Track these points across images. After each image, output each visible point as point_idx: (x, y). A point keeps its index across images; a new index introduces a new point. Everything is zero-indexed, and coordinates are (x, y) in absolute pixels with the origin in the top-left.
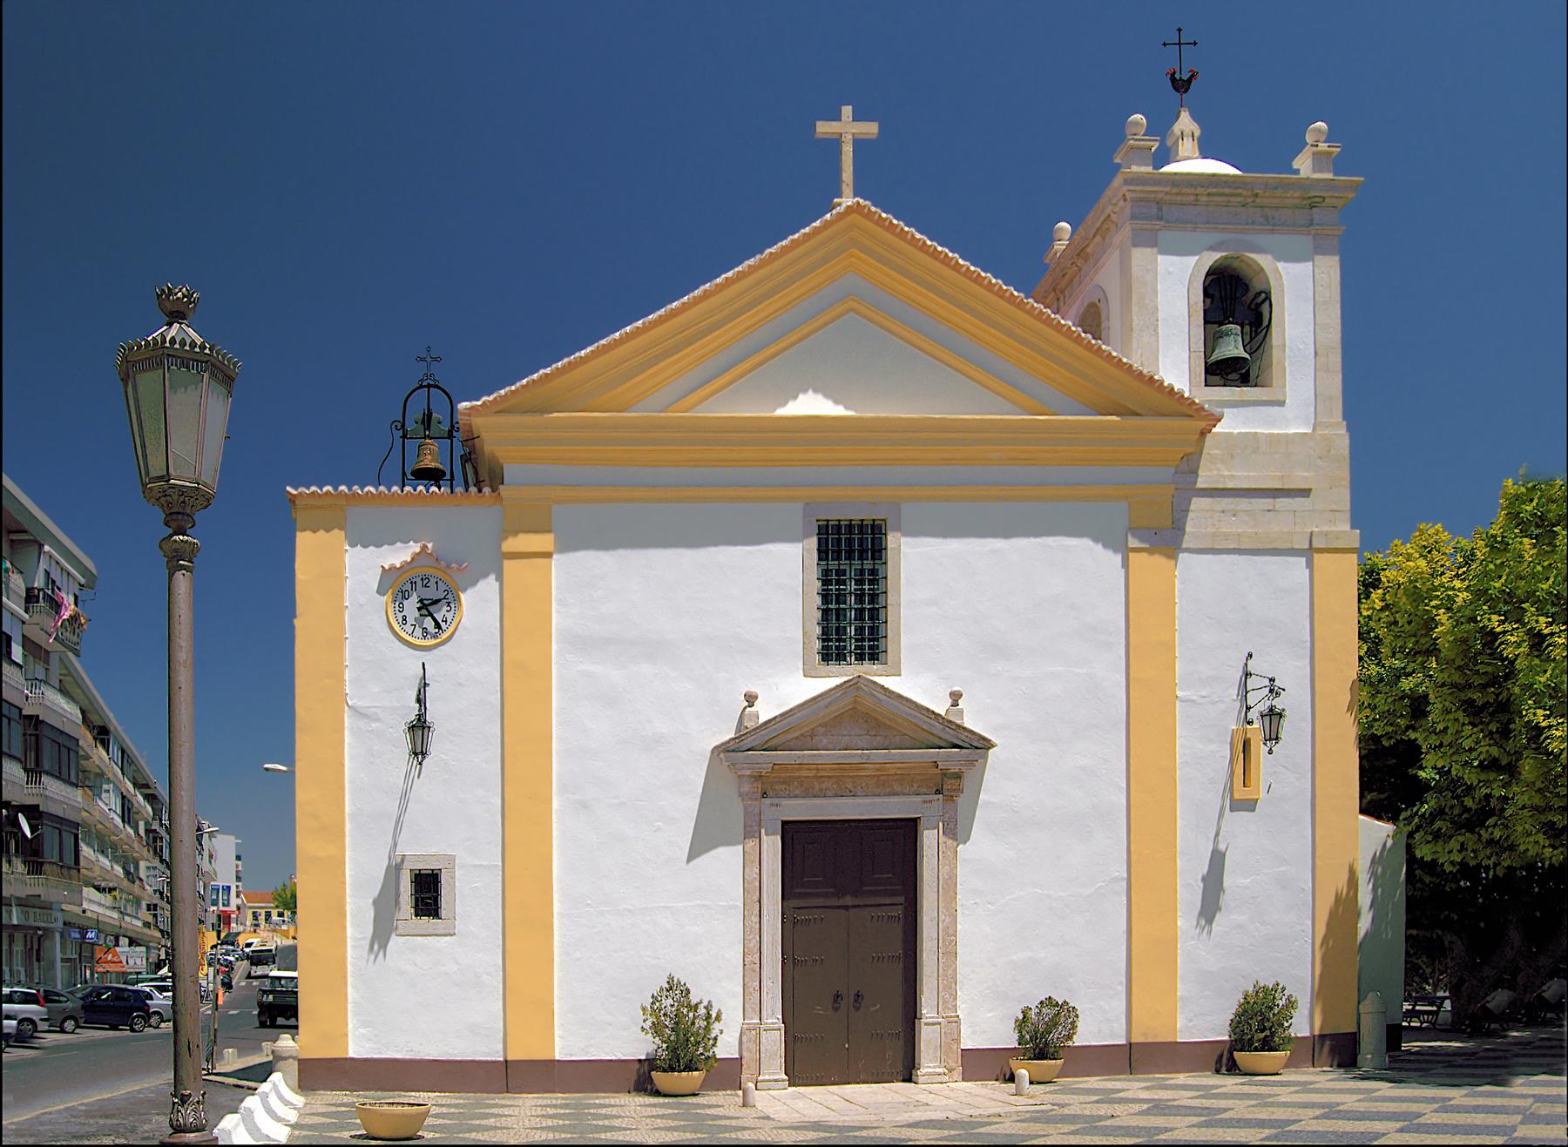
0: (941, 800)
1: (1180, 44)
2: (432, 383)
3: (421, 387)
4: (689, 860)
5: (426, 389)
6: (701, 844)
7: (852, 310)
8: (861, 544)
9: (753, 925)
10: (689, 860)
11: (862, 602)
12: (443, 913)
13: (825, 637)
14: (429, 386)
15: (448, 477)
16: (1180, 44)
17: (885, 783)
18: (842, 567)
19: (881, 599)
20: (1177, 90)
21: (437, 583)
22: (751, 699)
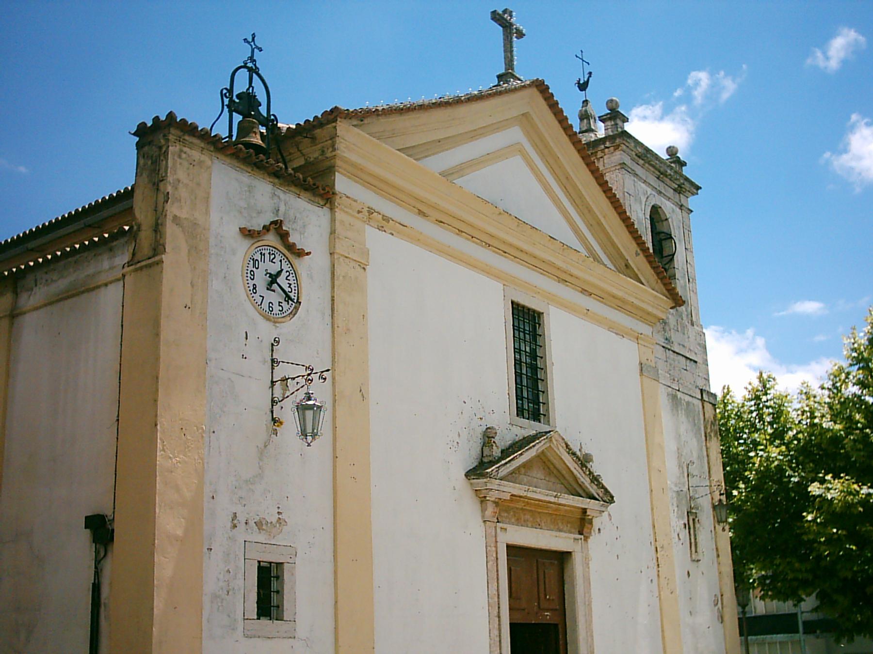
21: (281, 261)
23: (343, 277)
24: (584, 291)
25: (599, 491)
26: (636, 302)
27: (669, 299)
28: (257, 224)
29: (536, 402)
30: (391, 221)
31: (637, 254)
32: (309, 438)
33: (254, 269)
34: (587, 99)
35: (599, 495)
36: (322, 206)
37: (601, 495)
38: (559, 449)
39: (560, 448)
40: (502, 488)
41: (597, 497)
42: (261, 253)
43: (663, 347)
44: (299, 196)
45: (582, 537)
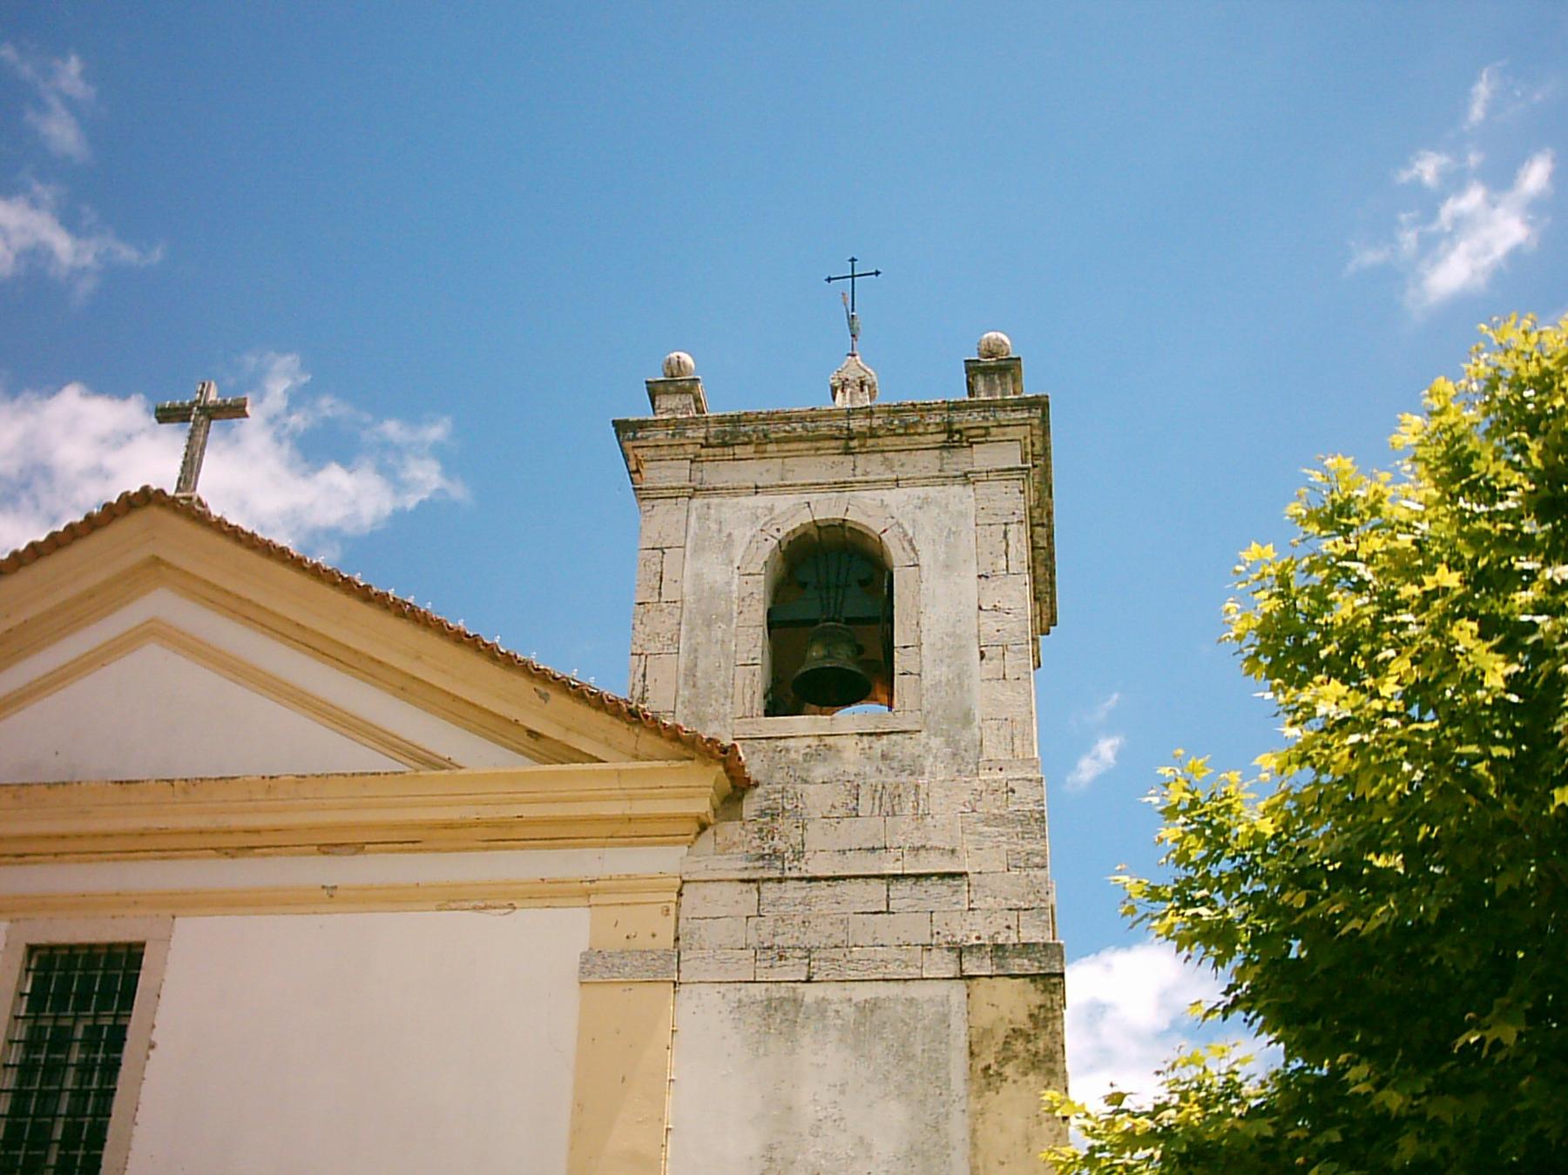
7: (153, 631)
16: (853, 276)
27: (692, 759)
31: (544, 697)
43: (743, 881)
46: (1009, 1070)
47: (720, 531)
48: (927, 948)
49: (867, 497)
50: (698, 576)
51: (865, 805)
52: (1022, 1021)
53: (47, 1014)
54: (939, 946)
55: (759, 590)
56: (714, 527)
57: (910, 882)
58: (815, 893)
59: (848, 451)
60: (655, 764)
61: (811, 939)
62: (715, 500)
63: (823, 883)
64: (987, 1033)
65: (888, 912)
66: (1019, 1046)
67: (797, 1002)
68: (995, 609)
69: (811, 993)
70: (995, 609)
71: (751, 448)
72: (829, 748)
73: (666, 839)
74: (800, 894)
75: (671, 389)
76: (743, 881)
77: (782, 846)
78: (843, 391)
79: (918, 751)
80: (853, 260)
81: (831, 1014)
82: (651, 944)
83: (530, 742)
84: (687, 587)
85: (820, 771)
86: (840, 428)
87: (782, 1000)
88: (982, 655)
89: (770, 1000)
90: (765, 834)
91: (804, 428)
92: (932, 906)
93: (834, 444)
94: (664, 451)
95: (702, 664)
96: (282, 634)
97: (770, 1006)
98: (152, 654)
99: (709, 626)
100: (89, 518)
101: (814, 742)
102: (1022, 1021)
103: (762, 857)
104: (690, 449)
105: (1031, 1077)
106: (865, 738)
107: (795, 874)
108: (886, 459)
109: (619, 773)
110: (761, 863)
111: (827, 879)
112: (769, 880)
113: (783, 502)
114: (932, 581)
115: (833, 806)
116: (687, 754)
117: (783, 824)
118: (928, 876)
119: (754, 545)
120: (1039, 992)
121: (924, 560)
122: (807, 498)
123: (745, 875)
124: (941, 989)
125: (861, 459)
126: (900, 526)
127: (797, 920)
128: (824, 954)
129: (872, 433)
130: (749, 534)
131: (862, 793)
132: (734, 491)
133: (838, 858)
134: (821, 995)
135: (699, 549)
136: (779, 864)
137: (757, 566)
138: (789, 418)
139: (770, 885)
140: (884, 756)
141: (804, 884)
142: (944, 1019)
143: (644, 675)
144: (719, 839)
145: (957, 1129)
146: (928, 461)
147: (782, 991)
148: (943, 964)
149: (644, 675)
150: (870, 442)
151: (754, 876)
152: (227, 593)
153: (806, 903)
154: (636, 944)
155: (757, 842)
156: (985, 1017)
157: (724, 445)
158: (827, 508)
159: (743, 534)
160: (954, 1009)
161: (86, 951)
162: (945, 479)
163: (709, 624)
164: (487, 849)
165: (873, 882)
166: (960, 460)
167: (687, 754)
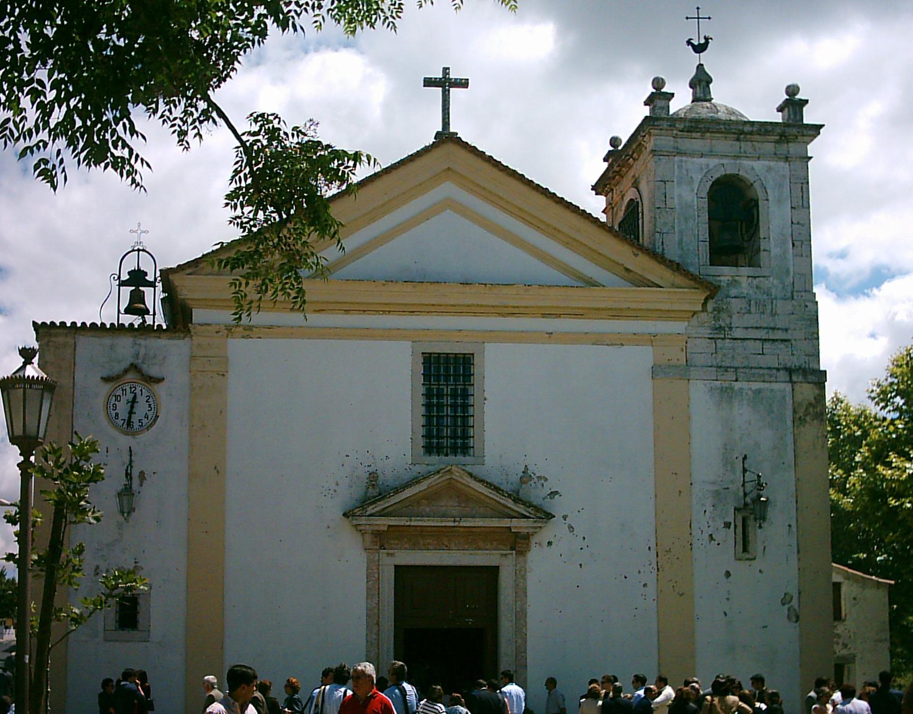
0: (514, 555)
1: (698, 18)
2: (141, 248)
3: (133, 250)
4: (823, 125)
5: (137, 252)
6: (817, 129)
7: (449, 204)
8: (455, 371)
9: (373, 641)
10: (823, 125)
11: (456, 412)
12: (140, 627)
13: (428, 436)
14: (139, 250)
15: (152, 313)
16: (698, 18)
17: (473, 538)
18: (441, 387)
19: (471, 410)
20: (696, 52)
21: (141, 390)
22: (711, 39)
23: (200, 388)
24: (544, 316)
25: (530, 510)
26: (632, 306)
27: (698, 288)
28: (118, 368)
29: (465, 436)
30: (254, 329)
31: (636, 255)
32: (126, 515)
33: (117, 403)
34: (702, 63)
35: (530, 513)
36: (184, 338)
37: (532, 512)
38: (463, 478)
39: (465, 477)
40: (372, 522)
41: (528, 514)
42: (123, 390)
43: (709, 338)
44: (159, 338)
45: (514, 552)
46: (808, 418)
47: (687, 175)
48: (778, 369)
49: (746, 163)
50: (680, 196)
51: (753, 309)
52: (812, 400)
53: (452, 383)
54: (782, 369)
55: (704, 204)
56: (685, 172)
57: (771, 342)
58: (736, 345)
59: (738, 140)
60: (685, 290)
61: (736, 364)
62: (684, 158)
63: (739, 341)
64: (800, 404)
65: (763, 354)
66: (811, 410)
67: (732, 389)
68: (798, 223)
69: (737, 385)
70: (798, 223)
71: (699, 134)
72: (736, 281)
73: (680, 319)
74: (730, 345)
75: (662, 97)
76: (709, 338)
77: (723, 325)
78: (700, 86)
79: (770, 285)
80: (698, 8)
81: (744, 394)
82: (679, 363)
83: (623, 272)
84: (676, 201)
85: (733, 292)
86: (739, 130)
87: (727, 388)
88: (793, 245)
89: (722, 387)
90: (716, 318)
91: (725, 128)
92: (778, 351)
93: (733, 136)
94: (663, 132)
95: (684, 239)
96: (511, 212)
97: (723, 390)
98: (448, 215)
99: (686, 222)
100: (584, 211)
101: (730, 279)
102: (812, 400)
103: (716, 329)
104: (675, 132)
105: (815, 422)
106: (750, 279)
107: (730, 337)
108: (753, 145)
109: (670, 292)
110: (716, 332)
111: (740, 339)
112: (719, 338)
113: (713, 162)
114: (773, 208)
115: (741, 309)
116: (697, 286)
117: (724, 315)
118: (777, 340)
119: (702, 184)
120: (83, 165)
121: (770, 198)
122: (722, 161)
123: (711, 336)
124: (782, 385)
125: (743, 144)
126: (760, 179)
127: (730, 356)
128: (742, 370)
129: (751, 133)
130: (700, 177)
131: (752, 303)
132: (692, 155)
133: (745, 331)
134: (740, 386)
135: (679, 183)
136: (723, 332)
137: (704, 194)
138: (719, 123)
139: (720, 340)
140: (757, 287)
141: (732, 341)
142: (784, 398)
143: (662, 243)
144: (699, 320)
145: (789, 439)
146: (769, 147)
147: (726, 384)
148: (783, 375)
149: (662, 243)
150: (749, 136)
151: (714, 336)
152: (484, 189)
153: (733, 349)
154: (672, 363)
155: (713, 322)
156: (799, 398)
157: (688, 132)
158: (729, 167)
159: (698, 177)
160: (787, 394)
161: (462, 356)
162: (776, 156)
163: (686, 220)
164: (609, 319)
165: (757, 341)
166: (783, 149)
167: (697, 286)
